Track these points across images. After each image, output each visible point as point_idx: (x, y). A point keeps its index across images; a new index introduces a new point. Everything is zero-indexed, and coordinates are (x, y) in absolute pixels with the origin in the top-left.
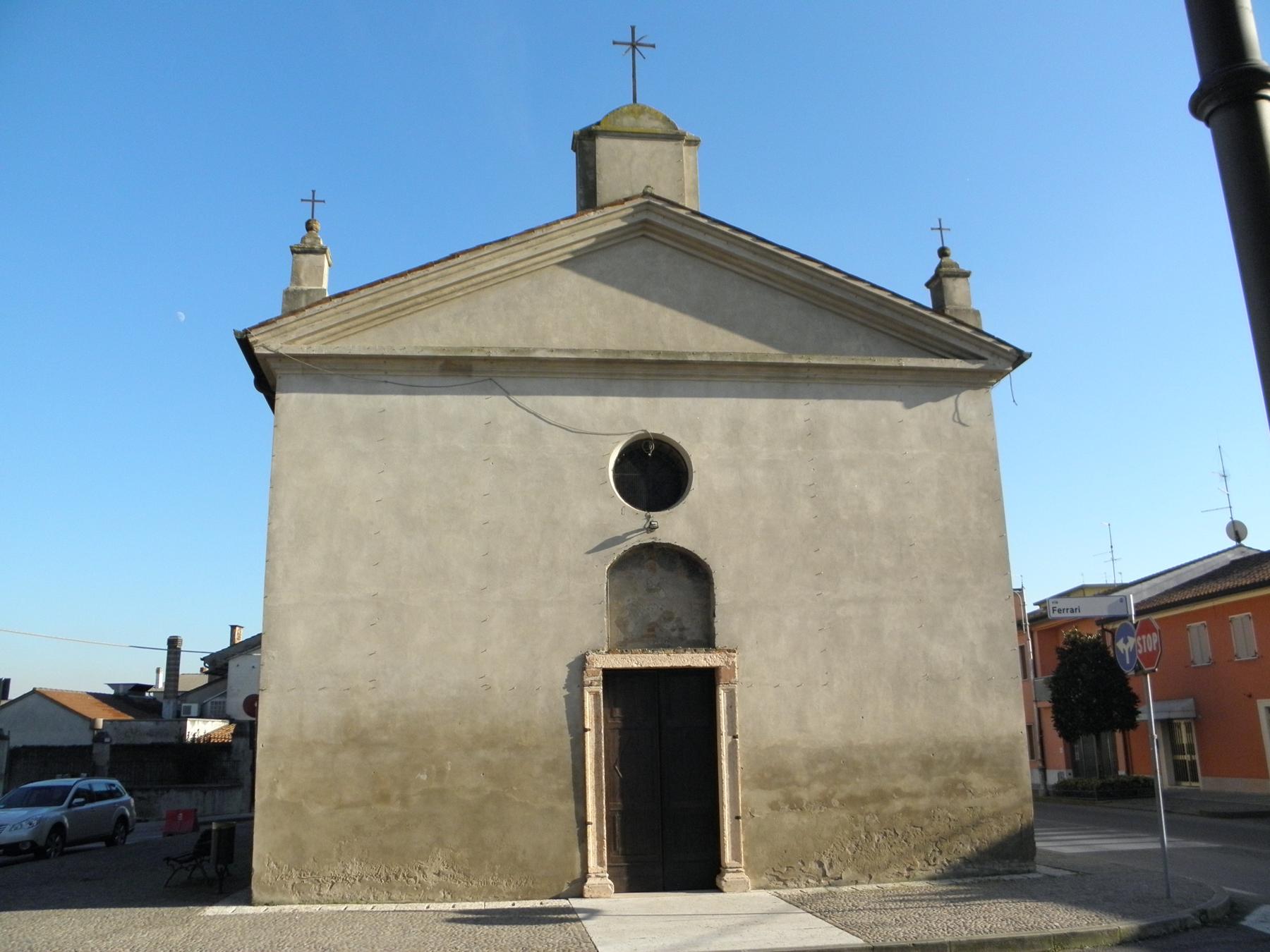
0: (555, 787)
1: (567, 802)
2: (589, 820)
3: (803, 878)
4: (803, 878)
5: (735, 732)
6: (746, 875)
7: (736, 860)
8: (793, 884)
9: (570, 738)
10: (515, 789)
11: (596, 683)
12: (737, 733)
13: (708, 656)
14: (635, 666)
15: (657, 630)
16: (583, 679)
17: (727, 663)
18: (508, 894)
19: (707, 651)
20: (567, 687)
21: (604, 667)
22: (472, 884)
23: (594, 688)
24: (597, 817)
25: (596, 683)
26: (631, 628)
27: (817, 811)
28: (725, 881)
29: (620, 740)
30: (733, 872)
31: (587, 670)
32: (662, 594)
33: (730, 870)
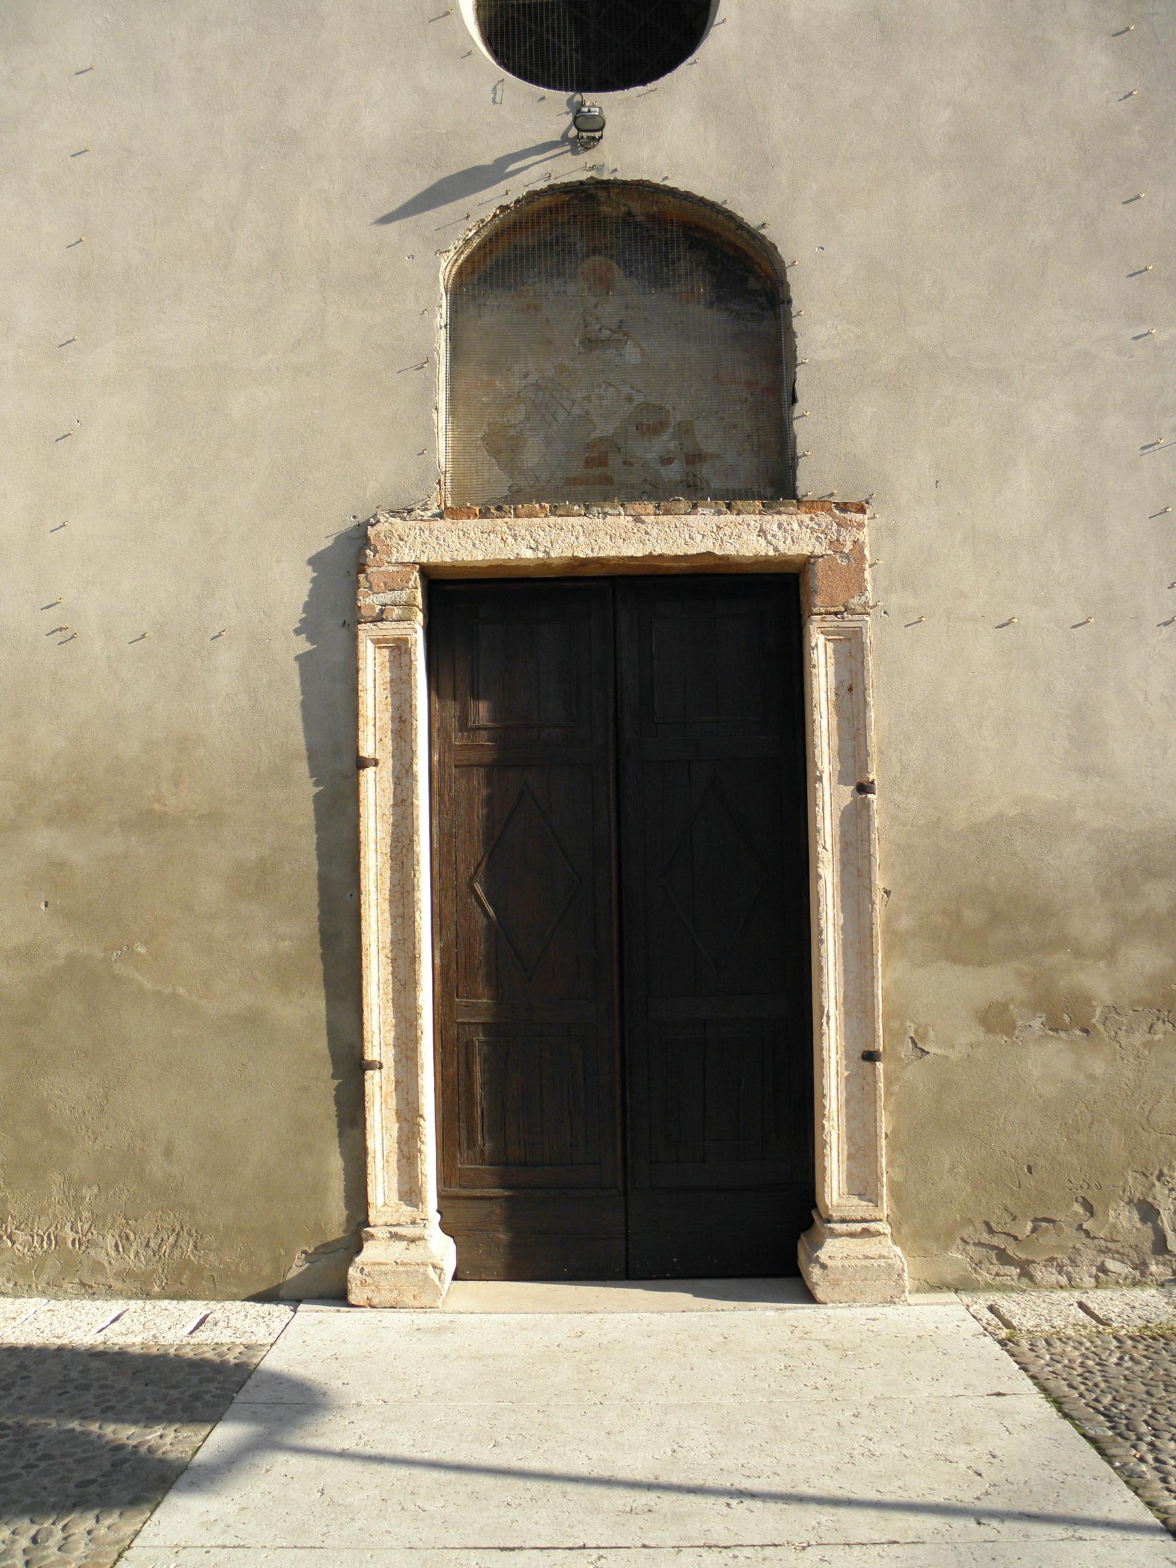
0: (262, 946)
1: (302, 995)
2: (372, 1053)
3: (1088, 1255)
4: (1088, 1255)
5: (865, 769)
6: (895, 1243)
7: (861, 1196)
8: (1050, 1276)
9: (316, 790)
10: (141, 950)
11: (397, 612)
12: (871, 777)
13: (771, 522)
14: (528, 554)
15: (615, 461)
16: (356, 599)
17: (836, 544)
18: (118, 1275)
19: (767, 508)
20: (307, 627)
21: (424, 559)
22: (13, 1243)
23: (389, 629)
24: (396, 1046)
25: (397, 612)
26: (531, 456)
27: (1138, 1038)
28: (824, 1267)
29: (489, 801)
30: (852, 1235)
31: (369, 570)
32: (632, 353)
33: (842, 1228)
